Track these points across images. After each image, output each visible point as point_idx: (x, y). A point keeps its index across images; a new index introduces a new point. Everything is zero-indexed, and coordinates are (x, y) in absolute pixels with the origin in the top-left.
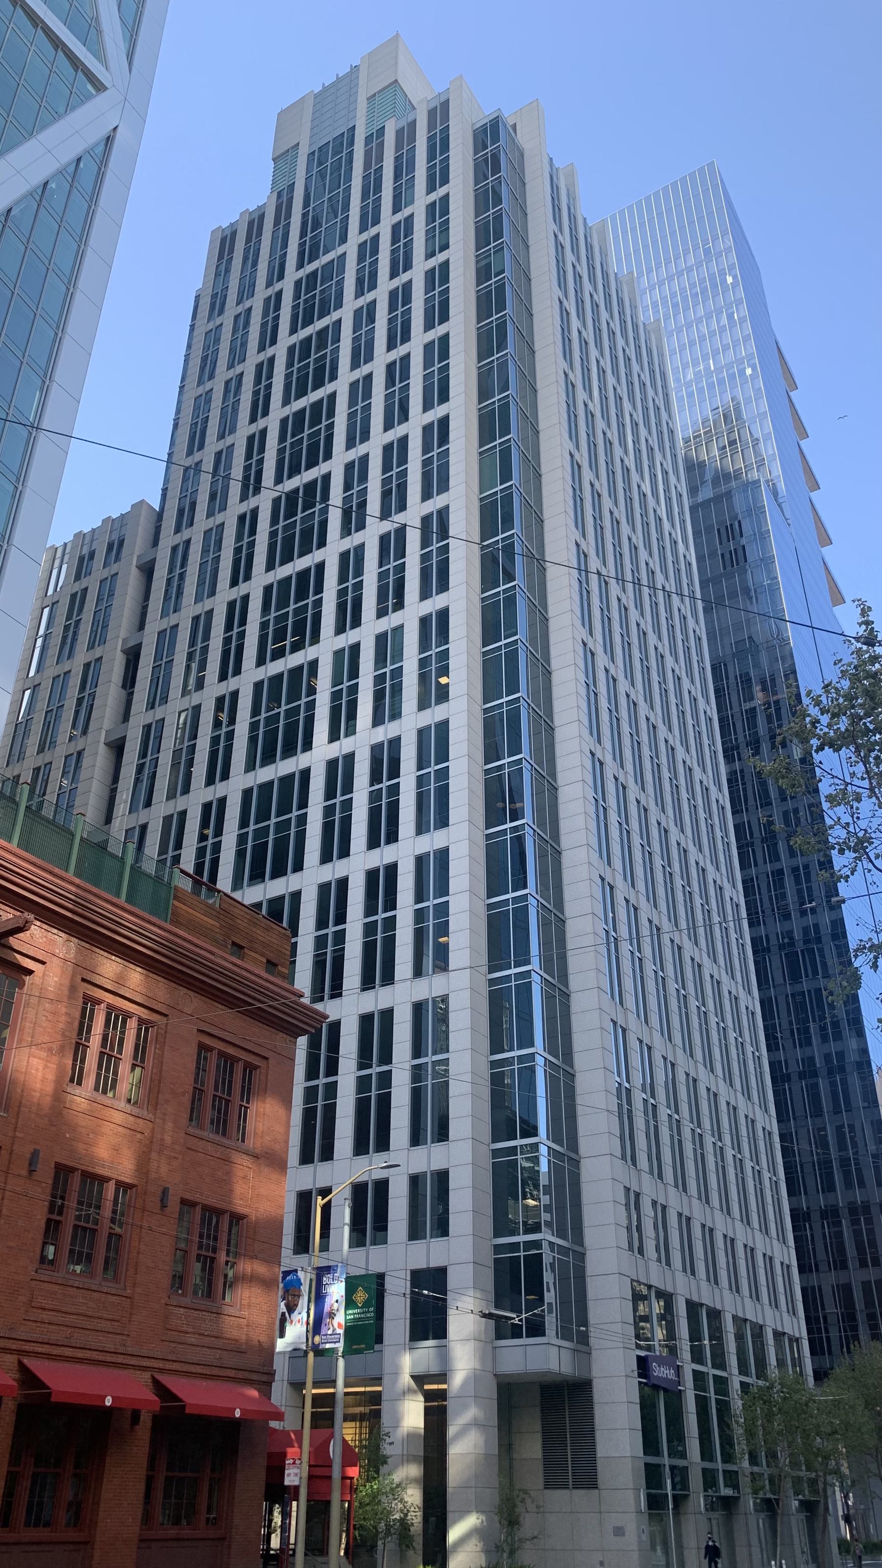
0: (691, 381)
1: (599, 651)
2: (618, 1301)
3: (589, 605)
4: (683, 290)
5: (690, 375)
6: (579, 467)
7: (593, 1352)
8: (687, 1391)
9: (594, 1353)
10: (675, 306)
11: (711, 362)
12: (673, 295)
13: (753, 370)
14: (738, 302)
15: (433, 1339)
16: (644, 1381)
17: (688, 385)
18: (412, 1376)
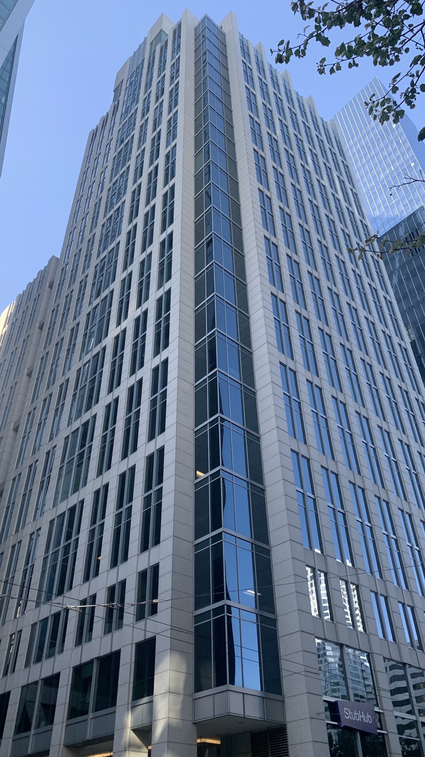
0: (383, 179)
1: (410, 389)
2: (301, 653)
3: (398, 364)
4: (371, 139)
5: (382, 176)
6: (360, 277)
7: (286, 700)
8: (390, 735)
9: (287, 701)
10: (369, 148)
11: (392, 167)
12: (367, 143)
13: (414, 163)
14: (401, 135)
15: (148, 696)
16: (336, 723)
17: (382, 181)
18: (132, 730)
